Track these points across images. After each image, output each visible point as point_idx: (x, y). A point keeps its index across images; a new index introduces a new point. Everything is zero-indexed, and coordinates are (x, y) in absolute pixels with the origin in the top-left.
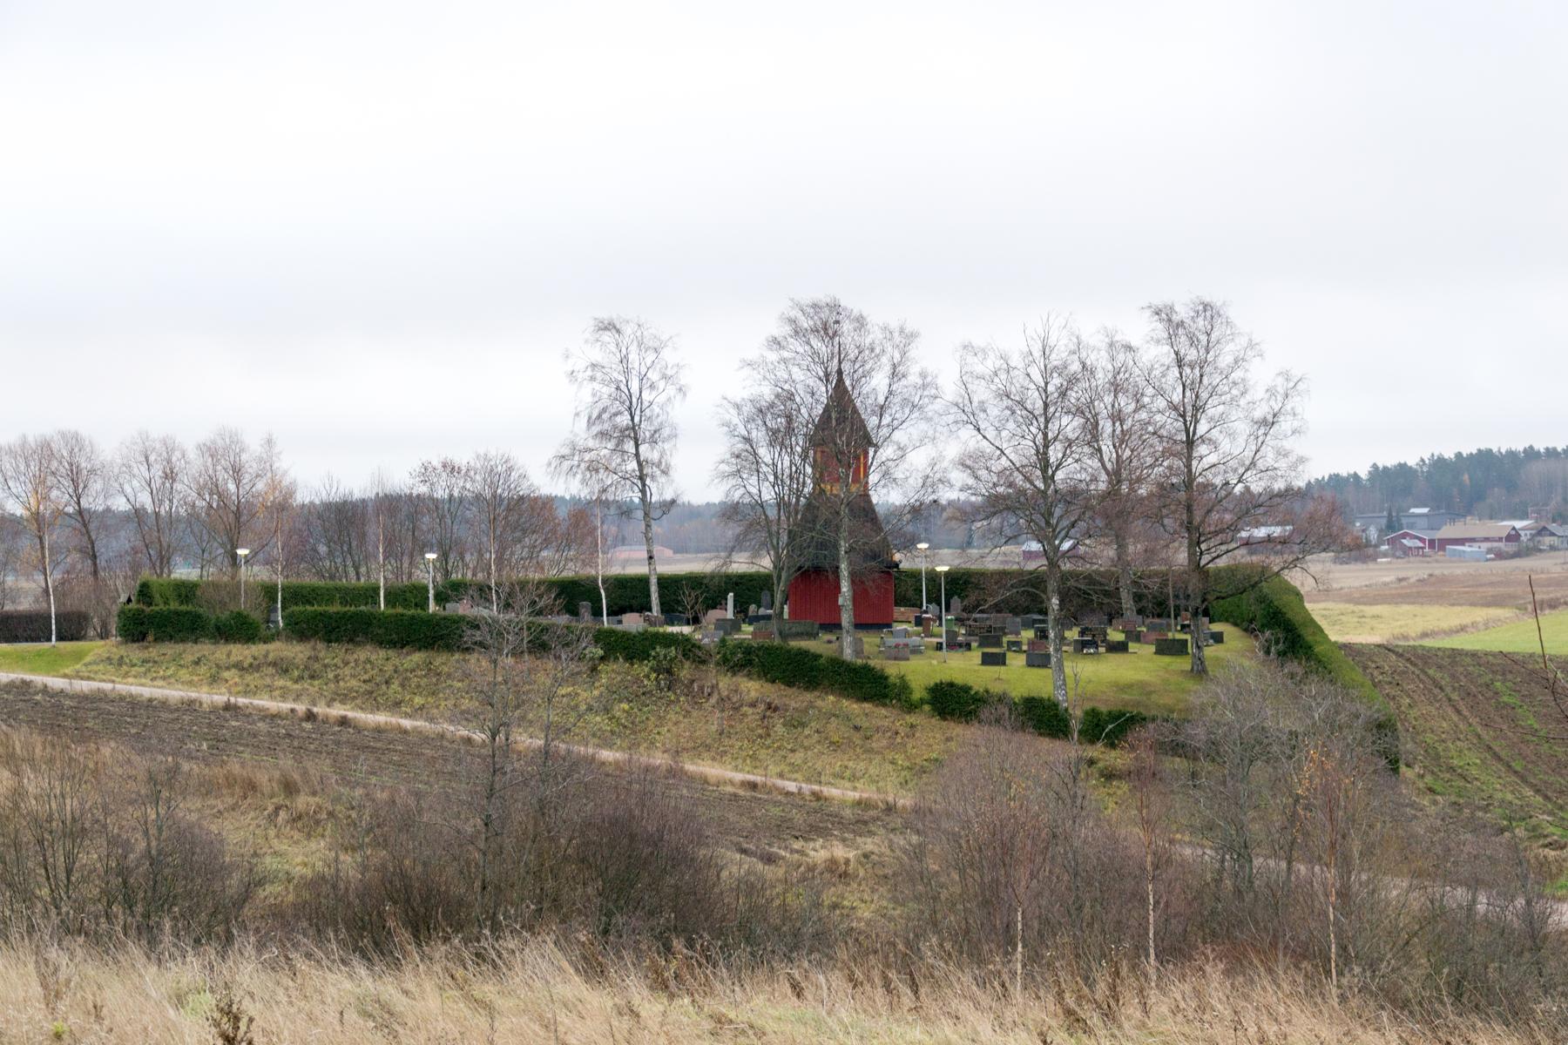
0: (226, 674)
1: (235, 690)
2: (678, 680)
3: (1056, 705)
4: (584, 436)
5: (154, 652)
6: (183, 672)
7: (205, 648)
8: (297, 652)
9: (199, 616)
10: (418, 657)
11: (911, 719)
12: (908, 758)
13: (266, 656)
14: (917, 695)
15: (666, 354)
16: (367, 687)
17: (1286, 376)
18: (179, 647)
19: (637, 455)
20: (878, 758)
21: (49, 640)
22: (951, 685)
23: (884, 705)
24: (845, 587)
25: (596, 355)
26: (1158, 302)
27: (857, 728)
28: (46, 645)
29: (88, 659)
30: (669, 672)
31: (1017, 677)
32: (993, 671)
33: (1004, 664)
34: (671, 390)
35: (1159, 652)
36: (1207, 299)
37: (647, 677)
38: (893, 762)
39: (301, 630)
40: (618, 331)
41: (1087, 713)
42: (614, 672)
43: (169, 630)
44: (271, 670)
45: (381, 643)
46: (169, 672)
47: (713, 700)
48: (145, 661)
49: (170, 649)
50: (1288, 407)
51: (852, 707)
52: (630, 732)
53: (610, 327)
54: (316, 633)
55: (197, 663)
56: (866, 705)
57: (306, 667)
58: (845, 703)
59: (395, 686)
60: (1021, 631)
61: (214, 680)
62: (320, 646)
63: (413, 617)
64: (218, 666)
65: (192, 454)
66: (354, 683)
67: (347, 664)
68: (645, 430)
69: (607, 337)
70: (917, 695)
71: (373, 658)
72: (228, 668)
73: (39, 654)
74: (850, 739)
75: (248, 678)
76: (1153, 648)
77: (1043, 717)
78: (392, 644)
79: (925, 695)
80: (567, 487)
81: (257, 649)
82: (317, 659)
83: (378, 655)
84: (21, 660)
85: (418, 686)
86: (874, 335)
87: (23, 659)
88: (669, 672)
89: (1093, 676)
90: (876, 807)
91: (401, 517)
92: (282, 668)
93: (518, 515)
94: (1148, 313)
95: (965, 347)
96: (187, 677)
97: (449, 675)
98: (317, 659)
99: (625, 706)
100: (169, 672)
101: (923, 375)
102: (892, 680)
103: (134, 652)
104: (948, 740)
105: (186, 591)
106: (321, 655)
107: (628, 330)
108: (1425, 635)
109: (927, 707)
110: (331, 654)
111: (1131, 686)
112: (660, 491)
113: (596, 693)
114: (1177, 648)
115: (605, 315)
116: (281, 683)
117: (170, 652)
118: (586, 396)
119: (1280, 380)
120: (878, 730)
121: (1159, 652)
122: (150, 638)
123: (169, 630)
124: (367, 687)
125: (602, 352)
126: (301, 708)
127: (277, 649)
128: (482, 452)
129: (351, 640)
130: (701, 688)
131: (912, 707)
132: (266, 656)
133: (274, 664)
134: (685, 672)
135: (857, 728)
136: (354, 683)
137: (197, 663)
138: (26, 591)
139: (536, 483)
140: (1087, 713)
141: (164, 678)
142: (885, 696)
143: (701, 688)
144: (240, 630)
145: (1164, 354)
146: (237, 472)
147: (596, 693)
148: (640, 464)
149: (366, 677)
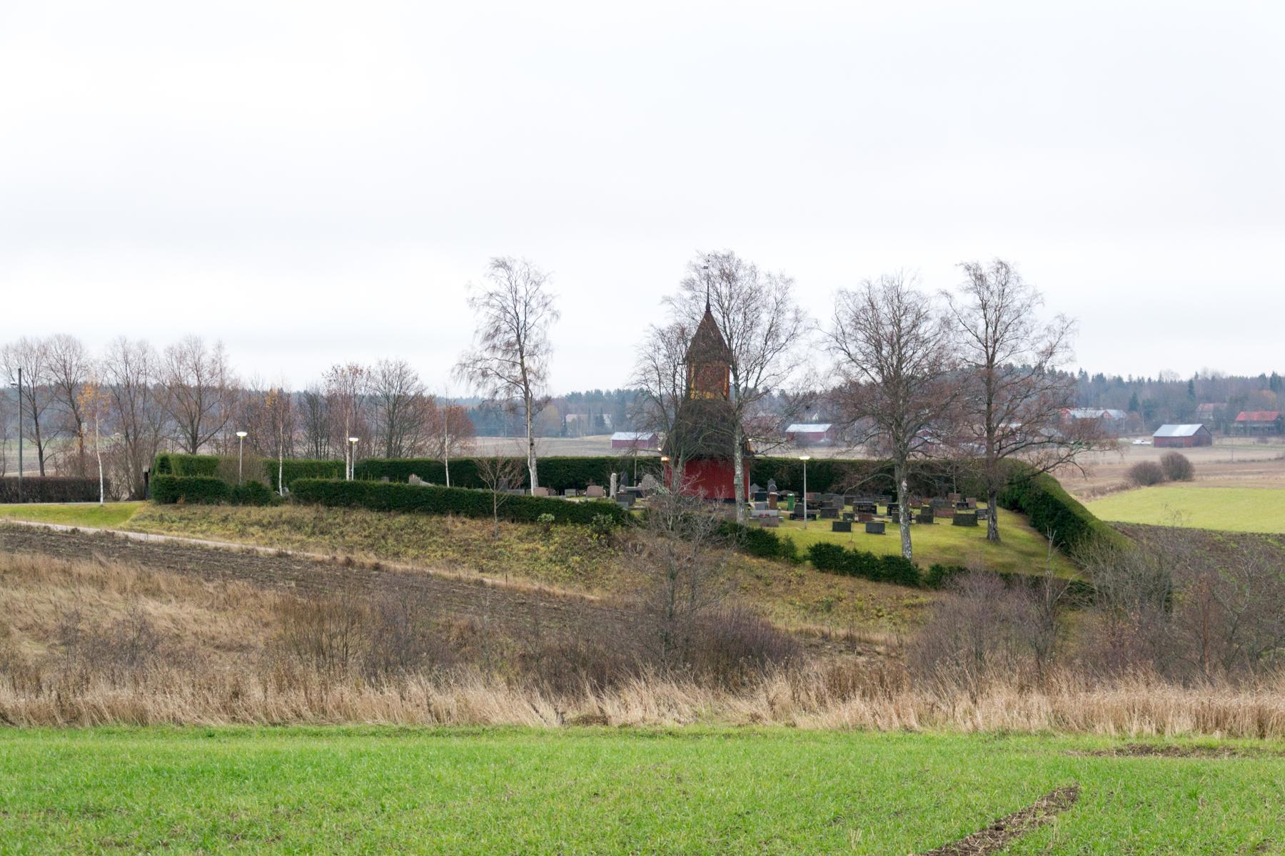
0: (252, 530)
1: (262, 542)
2: (614, 539)
3: (908, 561)
4: (480, 348)
5: (186, 511)
6: (214, 527)
7: (227, 509)
8: (306, 513)
9: (222, 484)
10: (403, 519)
11: (798, 571)
12: (802, 600)
13: (280, 516)
14: (800, 554)
15: (545, 288)
16: (370, 541)
17: (1062, 318)
18: (207, 508)
19: (522, 364)
20: (779, 601)
21: (98, 500)
22: (828, 546)
23: (775, 560)
24: (739, 471)
25: (492, 286)
26: (970, 260)
27: (758, 577)
28: (94, 505)
29: (134, 516)
30: (607, 533)
31: (888, 543)
32: (875, 539)
33: (849, 530)
34: (547, 315)
35: (955, 523)
36: (1003, 260)
37: (591, 536)
38: (791, 603)
39: (305, 496)
40: (509, 269)
41: (933, 569)
42: (561, 534)
43: (196, 494)
44: (286, 527)
45: (371, 507)
46: (204, 527)
47: (644, 555)
48: (181, 519)
49: (199, 509)
50: (1062, 342)
51: (749, 560)
52: (588, 579)
53: (502, 264)
54: (319, 498)
55: (225, 520)
56: (762, 560)
57: (315, 526)
58: (747, 558)
59: (391, 541)
60: (862, 504)
61: (242, 534)
62: (322, 509)
63: (398, 488)
64: (242, 523)
65: (163, 356)
66: (356, 538)
67: (347, 523)
68: (528, 346)
69: (501, 272)
70: (800, 554)
71: (368, 519)
72: (252, 525)
73: (92, 512)
74: (755, 587)
75: (270, 534)
76: (951, 521)
77: (896, 571)
78: (381, 509)
79: (807, 552)
80: (463, 391)
81: (268, 512)
82: (321, 519)
83: (372, 517)
84: (78, 515)
85: (410, 541)
86: (762, 281)
87: (80, 516)
88: (607, 533)
89: (934, 539)
90: (814, 636)
91: (322, 412)
92: (296, 525)
93: (408, 410)
94: (962, 268)
95: (841, 292)
96: (220, 532)
97: (432, 534)
98: (321, 519)
99: (577, 558)
100: (204, 527)
101: (797, 311)
102: (781, 541)
103: (169, 511)
104: (829, 587)
105: (209, 465)
106: (325, 515)
107: (516, 267)
108: (34, 573)
109: (808, 562)
110: (335, 516)
111: (948, 549)
112: (538, 393)
113: (552, 548)
114: (970, 521)
115: (501, 254)
116: (299, 537)
117: (199, 512)
118: (482, 319)
119: (1058, 321)
120: (775, 579)
121: (955, 523)
122: (181, 500)
123: (196, 494)
124: (370, 541)
125: (498, 284)
126: (341, 558)
127: (287, 511)
128: (383, 359)
129: (348, 505)
130: (635, 546)
131: (796, 562)
132: (280, 516)
133: (289, 523)
134: (618, 532)
135: (758, 577)
136: (356, 538)
137: (225, 520)
138: (23, 458)
139: (426, 384)
140: (933, 569)
141: (202, 532)
142: (776, 554)
143: (635, 546)
144: (255, 495)
145: (972, 300)
146: (197, 369)
147: (552, 548)
148: (524, 371)
149: (366, 533)
